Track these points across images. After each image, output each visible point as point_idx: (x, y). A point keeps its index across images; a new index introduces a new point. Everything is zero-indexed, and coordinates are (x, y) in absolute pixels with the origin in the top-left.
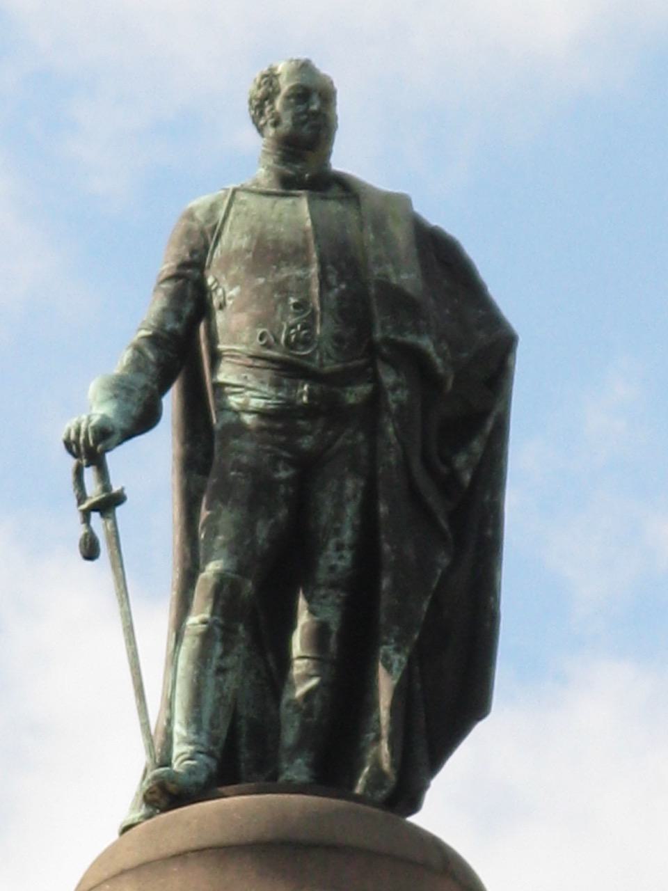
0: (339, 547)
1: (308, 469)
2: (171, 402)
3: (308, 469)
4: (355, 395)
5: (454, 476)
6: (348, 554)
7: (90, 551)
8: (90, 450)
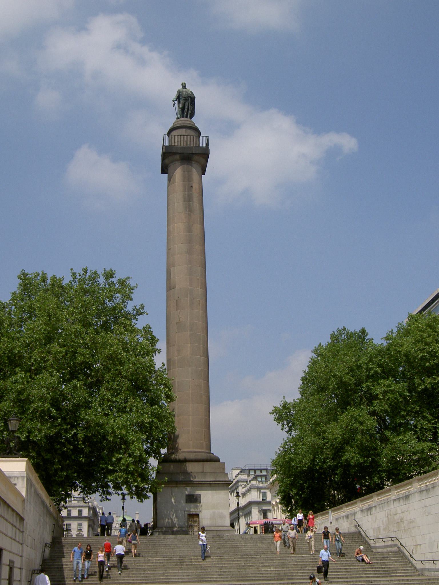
1: (185, 103)
3: (185, 103)
8: (173, 101)
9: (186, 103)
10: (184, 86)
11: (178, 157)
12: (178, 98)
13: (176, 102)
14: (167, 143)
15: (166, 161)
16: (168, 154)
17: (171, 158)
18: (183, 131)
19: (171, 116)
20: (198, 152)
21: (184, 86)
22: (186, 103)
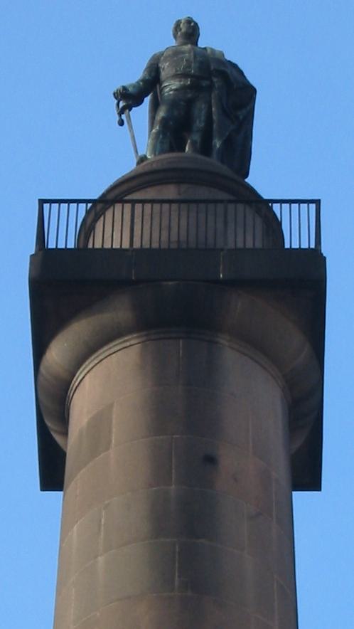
0: (200, 121)
2: (147, 100)
4: (205, 83)
6: (203, 124)
7: (121, 123)
10: (190, 32)
14: (63, 236)
15: (57, 352)
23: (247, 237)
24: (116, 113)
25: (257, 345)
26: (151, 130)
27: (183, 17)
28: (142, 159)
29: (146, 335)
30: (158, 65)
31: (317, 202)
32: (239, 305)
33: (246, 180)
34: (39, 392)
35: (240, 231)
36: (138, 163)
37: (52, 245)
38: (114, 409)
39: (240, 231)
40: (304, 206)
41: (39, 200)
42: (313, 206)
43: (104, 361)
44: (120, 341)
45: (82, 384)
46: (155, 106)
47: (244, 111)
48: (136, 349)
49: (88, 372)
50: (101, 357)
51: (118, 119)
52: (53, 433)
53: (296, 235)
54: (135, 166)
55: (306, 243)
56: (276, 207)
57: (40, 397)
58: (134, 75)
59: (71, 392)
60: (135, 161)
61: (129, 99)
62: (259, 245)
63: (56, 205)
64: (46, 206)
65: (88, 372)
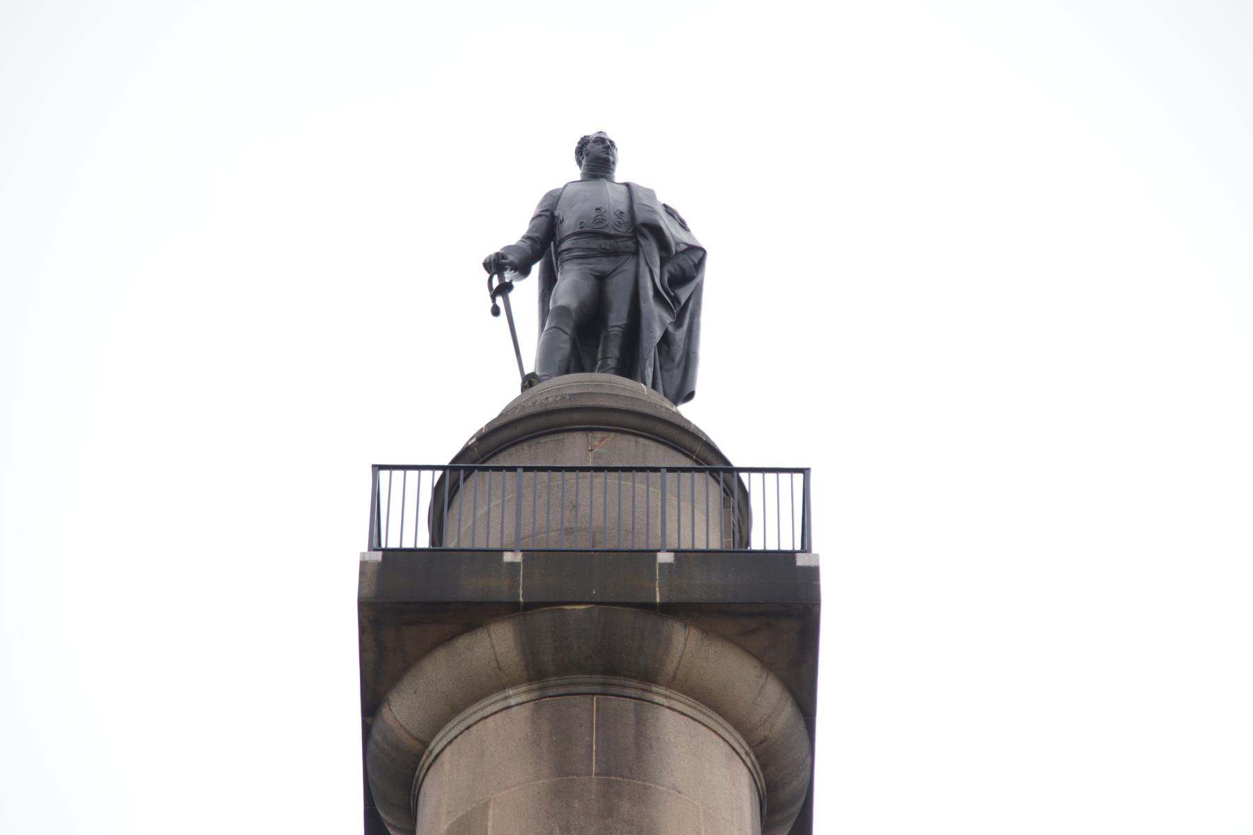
2: (536, 268)
5: (676, 299)
7: (496, 311)
9: (614, 283)
10: (596, 157)
11: (497, 643)
12: (546, 243)
13: (527, 290)
14: (410, 530)
15: (403, 709)
16: (407, 612)
17: (437, 673)
18: (575, 449)
19: (486, 362)
20: (701, 586)
21: (596, 157)
22: (614, 283)
23: (694, 524)
24: (487, 294)
25: (711, 702)
26: (543, 325)
27: (591, 132)
28: (529, 381)
29: (540, 689)
30: (552, 213)
31: (805, 471)
32: (685, 645)
33: (686, 410)
34: (369, 767)
35: (686, 506)
36: (524, 388)
37: (393, 543)
38: (491, 812)
39: (686, 506)
40: (785, 477)
41: (374, 466)
42: (799, 478)
43: (474, 727)
44: (498, 698)
45: (438, 761)
46: (548, 281)
47: (690, 288)
48: (520, 716)
49: (450, 743)
50: (470, 721)
51: (491, 305)
52: (389, 829)
53: (770, 530)
54: (519, 393)
55: (789, 542)
56: (744, 476)
57: (370, 773)
58: (513, 228)
59: (425, 761)
60: (518, 381)
61: (502, 268)
62: (715, 545)
63: (400, 473)
64: (384, 474)
65: (450, 743)
